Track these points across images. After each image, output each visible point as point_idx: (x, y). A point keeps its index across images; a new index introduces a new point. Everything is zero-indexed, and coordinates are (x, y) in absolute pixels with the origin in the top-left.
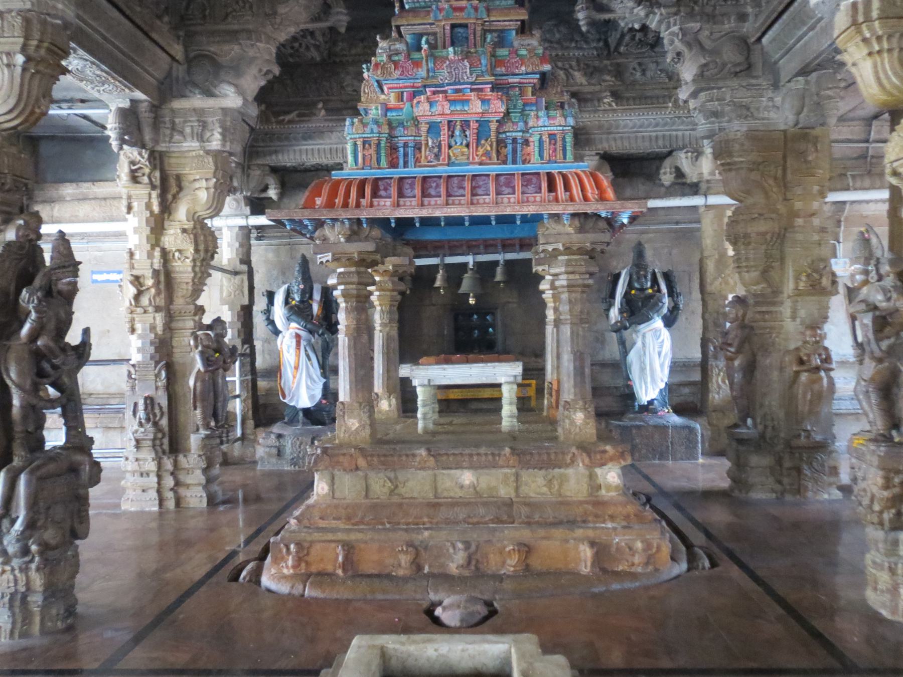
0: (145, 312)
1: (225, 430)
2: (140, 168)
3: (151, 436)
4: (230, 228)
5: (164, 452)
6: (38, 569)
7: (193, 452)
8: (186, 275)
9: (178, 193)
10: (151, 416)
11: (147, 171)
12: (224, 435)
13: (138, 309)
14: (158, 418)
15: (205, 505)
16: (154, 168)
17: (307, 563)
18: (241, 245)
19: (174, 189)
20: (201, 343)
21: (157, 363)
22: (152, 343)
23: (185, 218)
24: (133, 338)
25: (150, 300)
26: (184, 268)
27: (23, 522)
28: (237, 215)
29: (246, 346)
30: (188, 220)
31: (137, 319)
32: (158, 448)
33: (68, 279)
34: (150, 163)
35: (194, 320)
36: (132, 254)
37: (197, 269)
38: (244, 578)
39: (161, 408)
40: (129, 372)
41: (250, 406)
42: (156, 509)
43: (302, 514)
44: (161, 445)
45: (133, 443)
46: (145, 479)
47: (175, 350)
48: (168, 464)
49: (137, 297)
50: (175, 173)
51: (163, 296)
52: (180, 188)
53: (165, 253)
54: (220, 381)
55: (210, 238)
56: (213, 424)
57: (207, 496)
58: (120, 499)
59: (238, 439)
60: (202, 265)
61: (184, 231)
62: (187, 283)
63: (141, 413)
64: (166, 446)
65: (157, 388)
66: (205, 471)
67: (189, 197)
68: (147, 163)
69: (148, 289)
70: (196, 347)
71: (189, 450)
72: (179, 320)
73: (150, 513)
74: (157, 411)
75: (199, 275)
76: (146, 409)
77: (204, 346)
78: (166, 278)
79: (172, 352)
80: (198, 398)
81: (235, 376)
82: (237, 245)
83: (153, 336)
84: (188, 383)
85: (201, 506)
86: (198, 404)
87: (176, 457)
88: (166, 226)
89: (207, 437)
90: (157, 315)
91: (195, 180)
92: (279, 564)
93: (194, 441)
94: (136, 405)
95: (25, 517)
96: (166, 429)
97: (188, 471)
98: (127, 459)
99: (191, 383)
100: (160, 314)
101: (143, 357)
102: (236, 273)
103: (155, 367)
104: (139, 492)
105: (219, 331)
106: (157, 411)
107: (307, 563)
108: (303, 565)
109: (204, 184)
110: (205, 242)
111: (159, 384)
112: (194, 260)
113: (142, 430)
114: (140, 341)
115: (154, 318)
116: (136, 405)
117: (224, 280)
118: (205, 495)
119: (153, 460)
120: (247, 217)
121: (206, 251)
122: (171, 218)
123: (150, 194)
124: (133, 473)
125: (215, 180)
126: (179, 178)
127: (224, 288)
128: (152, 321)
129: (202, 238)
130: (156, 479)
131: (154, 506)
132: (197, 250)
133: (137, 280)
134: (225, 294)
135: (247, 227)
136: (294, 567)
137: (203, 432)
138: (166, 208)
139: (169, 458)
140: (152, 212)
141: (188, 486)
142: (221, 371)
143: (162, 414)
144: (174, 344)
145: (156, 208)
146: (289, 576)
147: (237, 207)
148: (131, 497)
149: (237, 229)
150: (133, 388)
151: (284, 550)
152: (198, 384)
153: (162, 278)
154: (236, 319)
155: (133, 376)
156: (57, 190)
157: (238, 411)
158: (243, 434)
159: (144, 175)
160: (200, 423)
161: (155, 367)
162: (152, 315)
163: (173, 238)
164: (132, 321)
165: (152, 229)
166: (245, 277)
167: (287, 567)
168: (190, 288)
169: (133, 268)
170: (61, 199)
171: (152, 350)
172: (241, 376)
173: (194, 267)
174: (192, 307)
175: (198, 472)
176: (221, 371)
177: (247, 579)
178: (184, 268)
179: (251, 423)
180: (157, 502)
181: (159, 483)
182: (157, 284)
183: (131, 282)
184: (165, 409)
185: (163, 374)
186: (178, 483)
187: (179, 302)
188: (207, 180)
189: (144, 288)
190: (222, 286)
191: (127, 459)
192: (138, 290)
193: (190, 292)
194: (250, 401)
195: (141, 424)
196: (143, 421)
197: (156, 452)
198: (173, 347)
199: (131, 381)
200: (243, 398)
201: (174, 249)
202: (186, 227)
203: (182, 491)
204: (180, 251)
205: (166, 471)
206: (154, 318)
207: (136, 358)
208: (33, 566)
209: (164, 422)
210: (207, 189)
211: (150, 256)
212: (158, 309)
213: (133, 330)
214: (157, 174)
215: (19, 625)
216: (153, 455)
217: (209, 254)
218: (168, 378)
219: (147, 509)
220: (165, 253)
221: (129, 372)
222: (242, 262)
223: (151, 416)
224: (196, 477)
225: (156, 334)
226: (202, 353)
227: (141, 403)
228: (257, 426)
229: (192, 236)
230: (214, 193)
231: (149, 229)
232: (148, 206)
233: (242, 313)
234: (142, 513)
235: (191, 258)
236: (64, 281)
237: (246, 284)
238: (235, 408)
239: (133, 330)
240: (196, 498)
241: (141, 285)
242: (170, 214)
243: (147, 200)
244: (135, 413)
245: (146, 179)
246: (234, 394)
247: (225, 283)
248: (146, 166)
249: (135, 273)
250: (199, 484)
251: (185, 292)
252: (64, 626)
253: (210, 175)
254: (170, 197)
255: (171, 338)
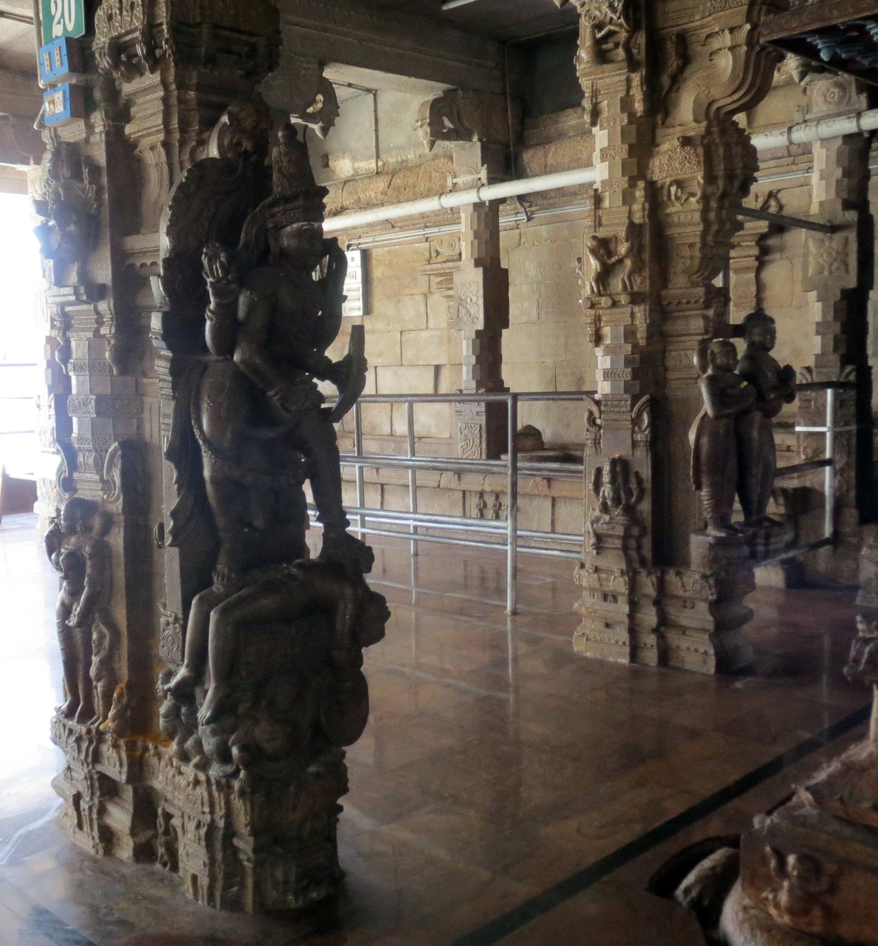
0: (615, 304)
1: (762, 533)
2: (611, 34)
3: (620, 531)
4: (824, 141)
5: (643, 562)
6: (242, 794)
7: (693, 567)
8: (689, 230)
9: (681, 69)
10: (623, 495)
11: (623, 35)
12: (760, 541)
13: (603, 300)
14: (633, 499)
15: (712, 671)
16: (633, 31)
17: (829, 913)
18: (847, 173)
19: (673, 63)
20: (713, 361)
21: (635, 399)
22: (628, 362)
23: (691, 118)
24: (599, 352)
25: (624, 282)
26: (686, 216)
27: (211, 701)
28: (839, 115)
29: (849, 368)
30: (696, 120)
31: (604, 318)
32: (633, 554)
33: (295, 226)
34: (627, 18)
35: (706, 318)
36: (598, 200)
37: (712, 216)
38: (687, 891)
39: (640, 481)
40: (591, 413)
41: (853, 482)
42: (625, 661)
43: (830, 782)
44: (639, 547)
45: (593, 540)
46: (610, 606)
47: (671, 375)
48: (648, 585)
49: (603, 277)
50: (675, 30)
51: (647, 272)
52: (686, 59)
53: (654, 193)
54: (755, 434)
55: (739, 150)
56: (738, 517)
57: (717, 654)
58: (571, 635)
59: (826, 542)
60: (720, 208)
61: (686, 141)
62: (691, 245)
63: (607, 489)
64: (647, 552)
65: (634, 444)
66: (715, 606)
67: (702, 74)
68: (622, 20)
69: (620, 261)
70: (704, 369)
71: (686, 563)
72: (678, 318)
73: (616, 665)
74: (633, 486)
75: (715, 228)
76: (613, 481)
77: (717, 368)
78: (653, 239)
79: (665, 380)
80: (704, 468)
81: (824, 425)
82: (838, 173)
83: (629, 348)
84: (686, 434)
85: (704, 670)
86: (705, 480)
87: (663, 573)
88: (658, 139)
89: (719, 543)
90: (636, 309)
91: (709, 36)
92: (760, 890)
93: (698, 545)
94: (599, 471)
95: (215, 695)
96: (649, 521)
97: (686, 603)
98: (582, 566)
99: (692, 436)
100: (642, 307)
101: (613, 387)
102: (833, 229)
103: (633, 406)
104: (600, 626)
105: (757, 338)
106: (633, 486)
107: (829, 913)
108: (817, 913)
109: (727, 39)
110: (730, 161)
111: (638, 437)
112: (705, 198)
113: (607, 518)
114: (608, 359)
115: (632, 315)
116: (599, 471)
117: (811, 244)
118: (712, 651)
119: (623, 573)
120: (859, 115)
121: (730, 177)
122: (668, 122)
123: (629, 81)
124: (592, 590)
125: (748, 27)
126: (683, 40)
127: (811, 259)
128: (628, 321)
129: (721, 151)
130: (626, 609)
131: (621, 655)
132: (710, 178)
133: (603, 247)
134: (811, 271)
135: (859, 134)
136: (790, 911)
137: (713, 532)
138: (659, 103)
139: (649, 574)
140: (631, 115)
141: (684, 630)
142: (757, 416)
143: (642, 492)
144: (670, 363)
145: (639, 107)
146: (779, 928)
147: (842, 98)
148: (587, 632)
149: (840, 142)
150: (596, 442)
151: (773, 863)
152: (705, 441)
153: (647, 240)
154: (830, 318)
155: (598, 421)
156: (556, 123)
157: (827, 490)
158: (836, 533)
159: (617, 45)
160: (707, 515)
161: (633, 406)
162: (628, 309)
163: (672, 162)
164: (598, 319)
165: (631, 148)
166: (852, 236)
167: (777, 906)
168: (697, 254)
169: (600, 225)
170: (561, 135)
171: (627, 374)
172: (835, 423)
173: (705, 211)
174: (700, 291)
175: (703, 607)
176: (757, 416)
177: (694, 893)
178: (686, 216)
179: (851, 515)
180: (627, 650)
181: (631, 616)
182: (636, 251)
183: (593, 252)
184: (648, 485)
185: (646, 418)
186: (664, 621)
187: (680, 285)
188: (732, 30)
189: (613, 260)
190: (806, 256)
191: (582, 566)
192: (603, 264)
193: (697, 262)
194: (853, 474)
195: (605, 508)
196: (609, 503)
197: (629, 561)
198: (666, 370)
199: (593, 429)
200: (838, 466)
201: (668, 180)
202: (691, 134)
203: (674, 638)
204: (680, 184)
205: (647, 596)
206: (632, 315)
207: (604, 388)
208: (236, 784)
209: (646, 506)
210: (731, 49)
211: (628, 198)
212: (635, 298)
213: (598, 339)
214: (641, 39)
215: (219, 885)
216: (623, 566)
217: (737, 183)
218: (652, 424)
219: (611, 659)
220: (654, 193)
221: (591, 413)
222: (847, 205)
223: (623, 495)
224: (698, 617)
225: (635, 346)
226: (712, 381)
227: (606, 468)
228: (864, 520)
229: (700, 150)
230: (748, 54)
231: (626, 147)
232: (626, 104)
233: (844, 304)
234: (602, 663)
235: (699, 194)
236: (288, 229)
237: (853, 247)
238: (823, 484)
239: (598, 339)
240: (697, 654)
241: (610, 254)
242: (667, 114)
243: (622, 94)
244: (597, 485)
245: (621, 53)
246: (822, 457)
247: (812, 247)
248: (621, 26)
249: (602, 233)
250: (703, 630)
251: (688, 262)
252: (300, 903)
253: (741, 18)
254: (666, 80)
255: (664, 352)
